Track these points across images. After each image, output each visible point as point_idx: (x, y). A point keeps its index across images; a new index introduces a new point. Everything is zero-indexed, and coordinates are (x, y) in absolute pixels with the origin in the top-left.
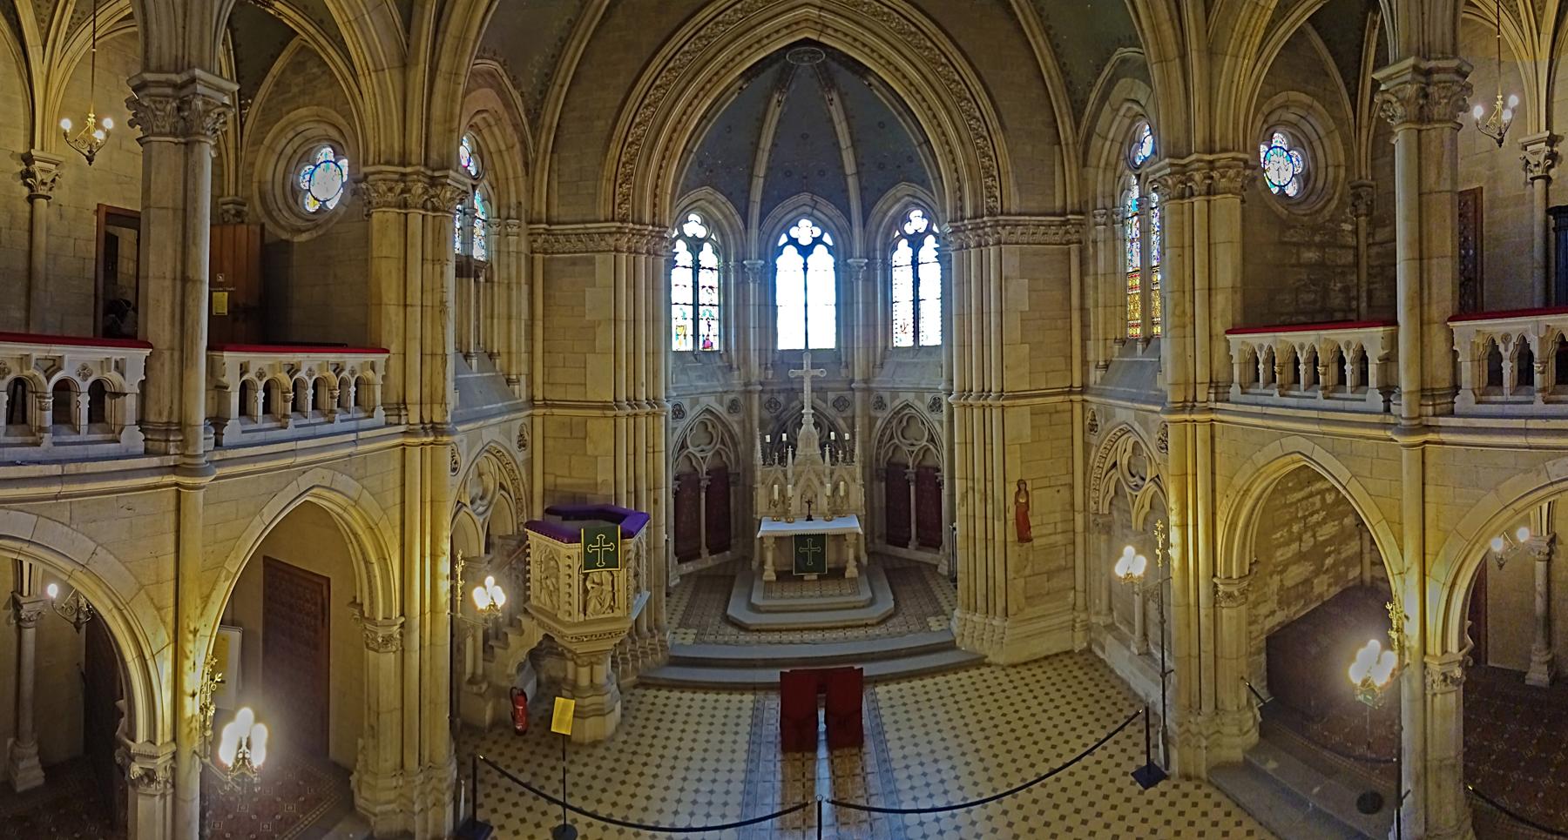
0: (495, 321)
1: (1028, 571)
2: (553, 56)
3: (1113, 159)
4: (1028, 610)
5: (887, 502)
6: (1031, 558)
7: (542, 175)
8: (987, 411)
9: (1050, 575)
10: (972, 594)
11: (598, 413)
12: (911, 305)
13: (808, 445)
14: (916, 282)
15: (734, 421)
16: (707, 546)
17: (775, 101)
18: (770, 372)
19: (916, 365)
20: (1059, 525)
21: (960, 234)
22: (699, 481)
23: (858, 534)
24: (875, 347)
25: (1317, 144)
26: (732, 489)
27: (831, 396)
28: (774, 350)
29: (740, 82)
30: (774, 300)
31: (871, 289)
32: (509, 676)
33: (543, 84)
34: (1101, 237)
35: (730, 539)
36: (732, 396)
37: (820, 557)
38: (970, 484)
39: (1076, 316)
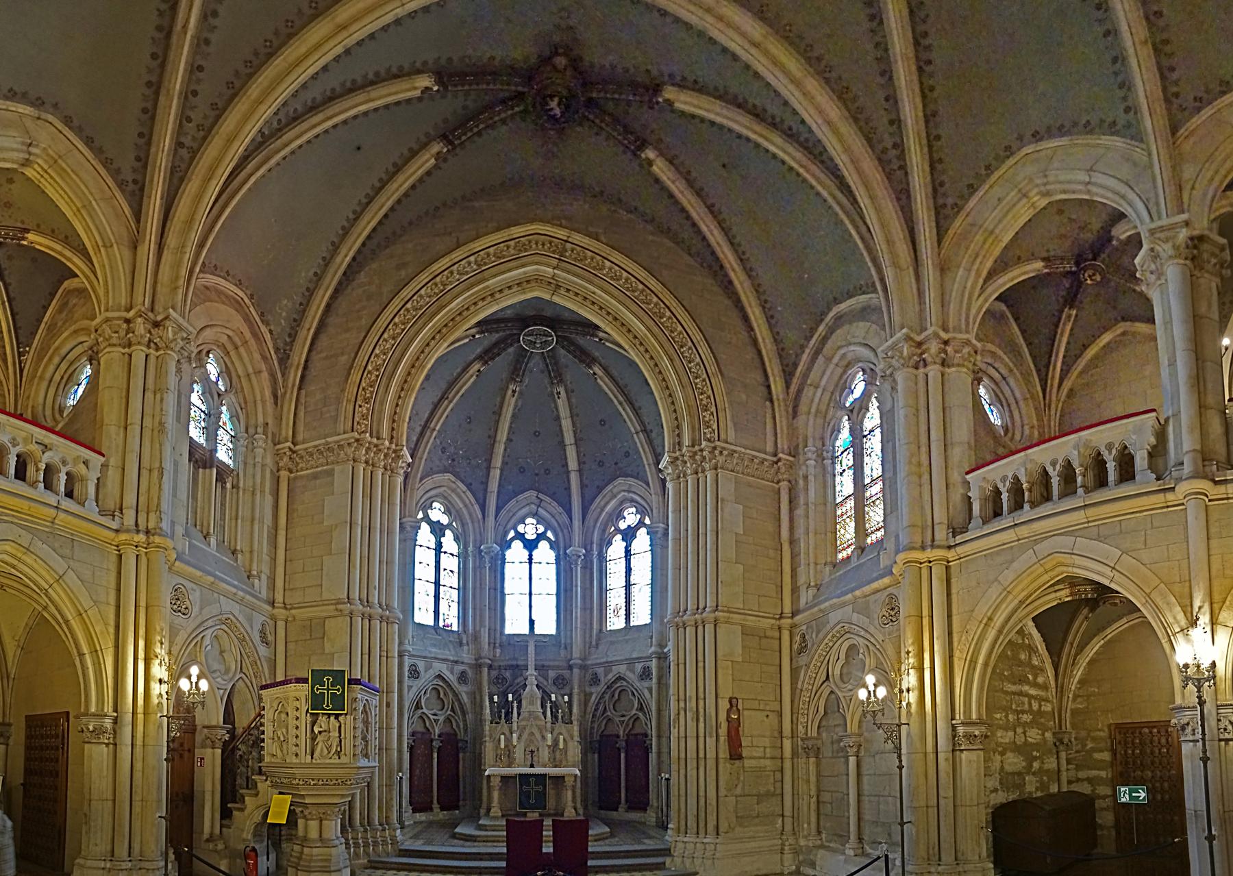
0: (239, 521)
1: (739, 791)
2: (301, 304)
3: (823, 408)
4: (738, 829)
5: (600, 773)
6: (742, 778)
7: (290, 405)
9: (760, 798)
10: (683, 816)
12: (623, 591)
13: (532, 703)
14: (629, 570)
15: (463, 691)
16: (438, 803)
17: (510, 392)
18: (498, 651)
19: (627, 641)
20: (768, 750)
22: (432, 741)
23: (576, 776)
24: (591, 628)
25: (1014, 406)
26: (461, 755)
27: (552, 674)
28: (502, 632)
29: (474, 331)
30: (503, 587)
31: (588, 577)
32: (244, 840)
33: (292, 328)
34: (812, 471)
35: (459, 801)
36: (460, 668)
37: (542, 796)
39: (786, 547)
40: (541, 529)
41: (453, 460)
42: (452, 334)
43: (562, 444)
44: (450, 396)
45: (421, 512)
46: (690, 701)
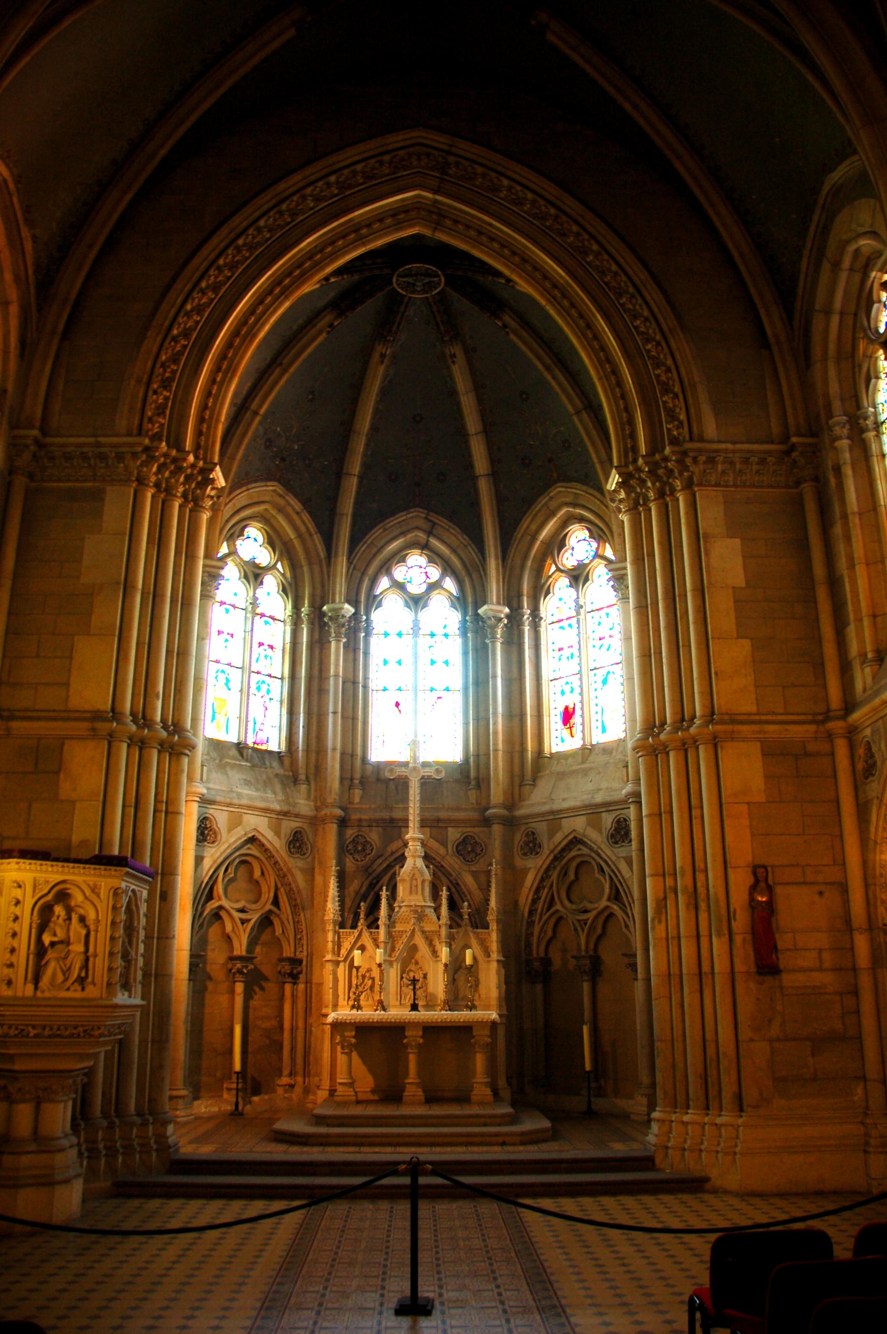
6: (779, 1008)
15: (295, 865)
18: (358, 793)
20: (826, 956)
27: (454, 834)
28: (364, 759)
36: (294, 824)
38: (669, 882)
41: (283, 460)
42: (298, 288)
43: (462, 433)
44: (286, 361)
45: (225, 544)
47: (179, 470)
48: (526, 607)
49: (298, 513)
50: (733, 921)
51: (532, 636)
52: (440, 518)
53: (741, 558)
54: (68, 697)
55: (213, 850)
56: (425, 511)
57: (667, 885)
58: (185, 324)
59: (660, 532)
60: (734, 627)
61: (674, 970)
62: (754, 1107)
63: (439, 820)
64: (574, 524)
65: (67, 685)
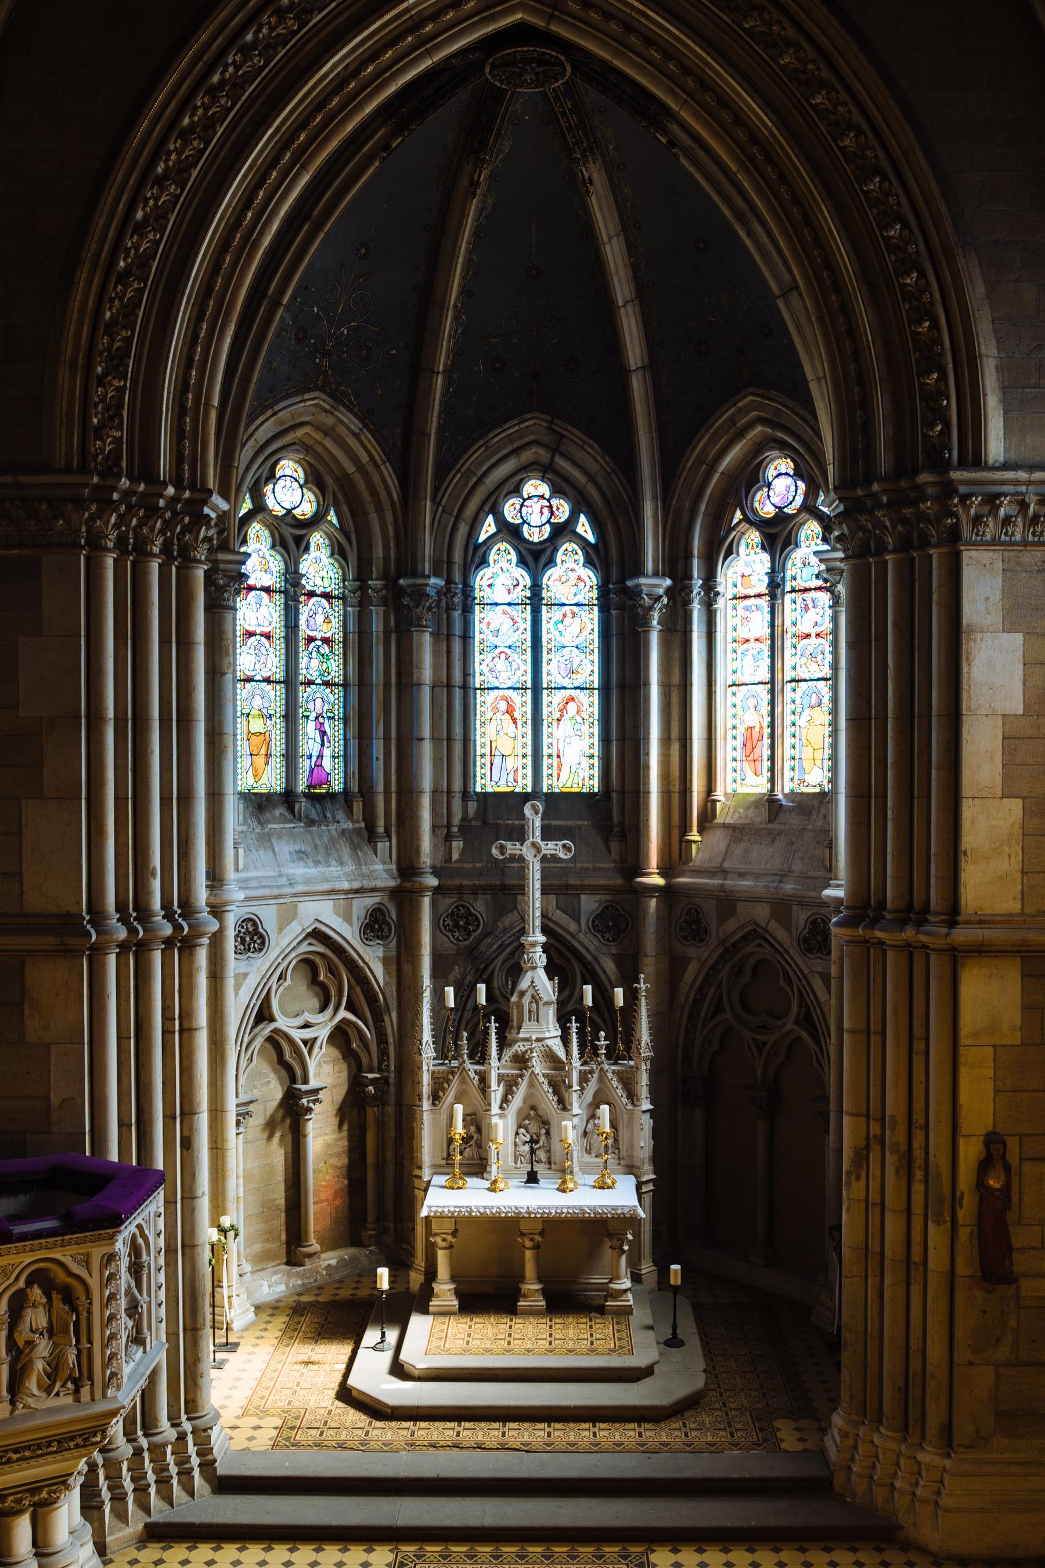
6: (1012, 1323)
8: (918, 958)
11: (49, 941)
18: (457, 845)
21: (863, 519)
27: (589, 904)
38: (875, 1129)
40: (563, 510)
46: (893, 1128)
47: (153, 511)
48: (695, 574)
49: (354, 434)
50: (958, 1209)
51: (704, 618)
52: (570, 428)
53: (1021, 666)
54: (22, 893)
55: (259, 961)
56: (549, 418)
57: (872, 1133)
58: (137, 249)
59: (898, 607)
60: (999, 780)
61: (874, 1246)
62: (967, 1448)
63: (568, 886)
64: (772, 449)
65: (20, 875)
